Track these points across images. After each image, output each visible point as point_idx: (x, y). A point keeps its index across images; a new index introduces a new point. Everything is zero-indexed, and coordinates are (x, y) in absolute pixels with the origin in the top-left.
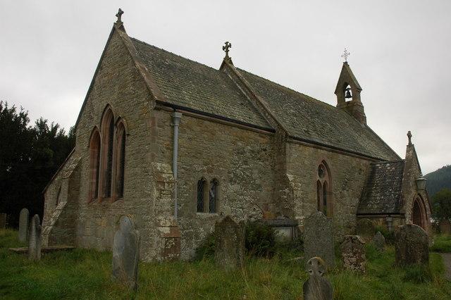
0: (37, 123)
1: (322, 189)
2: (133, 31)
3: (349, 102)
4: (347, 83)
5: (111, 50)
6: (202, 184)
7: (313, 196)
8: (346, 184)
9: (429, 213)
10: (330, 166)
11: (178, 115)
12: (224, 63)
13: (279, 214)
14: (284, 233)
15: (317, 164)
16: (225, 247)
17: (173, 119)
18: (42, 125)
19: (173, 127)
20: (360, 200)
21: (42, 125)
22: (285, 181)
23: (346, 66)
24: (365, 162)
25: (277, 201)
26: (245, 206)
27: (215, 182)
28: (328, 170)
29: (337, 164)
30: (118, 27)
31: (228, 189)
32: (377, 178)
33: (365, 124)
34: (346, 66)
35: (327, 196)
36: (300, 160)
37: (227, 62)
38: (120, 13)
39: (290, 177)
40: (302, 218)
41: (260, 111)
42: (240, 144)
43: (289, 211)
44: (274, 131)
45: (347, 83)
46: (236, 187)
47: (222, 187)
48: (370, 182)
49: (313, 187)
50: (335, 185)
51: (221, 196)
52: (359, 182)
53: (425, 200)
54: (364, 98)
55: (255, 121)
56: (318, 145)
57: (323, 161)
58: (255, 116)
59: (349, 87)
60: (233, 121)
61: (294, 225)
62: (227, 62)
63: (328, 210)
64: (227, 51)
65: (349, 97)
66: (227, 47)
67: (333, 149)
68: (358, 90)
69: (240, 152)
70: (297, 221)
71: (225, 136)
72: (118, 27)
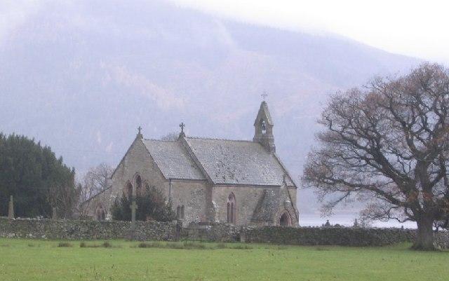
4: (262, 122)
23: (264, 103)
24: (259, 189)
25: (208, 214)
27: (183, 207)
30: (139, 136)
31: (188, 209)
32: (265, 202)
45: (262, 122)
47: (185, 208)
49: (225, 207)
56: (229, 185)
67: (238, 185)
72: (139, 136)
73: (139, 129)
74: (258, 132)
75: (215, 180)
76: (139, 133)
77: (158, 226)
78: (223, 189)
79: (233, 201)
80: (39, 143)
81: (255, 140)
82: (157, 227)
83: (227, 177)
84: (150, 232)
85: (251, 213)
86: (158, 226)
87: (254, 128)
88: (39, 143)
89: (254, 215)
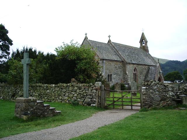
0: (35, 50)
1: (135, 75)
2: (90, 38)
3: (143, 46)
4: (143, 40)
5: (84, 44)
6: (109, 75)
7: (133, 77)
8: (141, 73)
9: (163, 79)
10: (137, 69)
11: (104, 61)
12: (109, 41)
13: (124, 81)
14: (127, 86)
15: (134, 69)
16: (117, 88)
17: (103, 62)
18: (39, 52)
19: (103, 64)
20: (145, 77)
21: (39, 52)
22: (126, 74)
23: (143, 34)
24: (147, 67)
25: (124, 78)
26: (117, 80)
27: (111, 75)
28: (137, 70)
29: (139, 68)
30: (86, 38)
31: (114, 76)
32: (150, 72)
33: (149, 53)
34: (143, 34)
35: (136, 77)
36: (130, 69)
37: (110, 41)
38: (86, 34)
39: (127, 73)
40: (130, 82)
41: (119, 56)
42: (151, 91)
43: (127, 81)
44: (123, 61)
45: (143, 40)
46: (115, 75)
47: (112, 76)
48: (148, 72)
49: (133, 75)
50: (138, 74)
51: (112, 78)
52: (145, 72)
53: (162, 77)
54: (149, 45)
55: (119, 59)
56: (134, 64)
57: (135, 68)
58: (118, 58)
59: (144, 41)
60: (114, 60)
61: (128, 84)
62: (109, 41)
63: (136, 81)
64: (109, 38)
65: (144, 44)
66: (109, 37)
67: (138, 64)
68: (147, 42)
69: (116, 67)
70: (129, 83)
71: (113, 64)
72: (86, 38)
73: (86, 34)
74: (141, 45)
75: (127, 60)
76: (86, 36)
77: (80, 88)
78: (132, 65)
79: (136, 72)
80: (17, 50)
81: (141, 48)
82: (78, 91)
83: (132, 60)
84: (71, 96)
85: (144, 77)
86: (80, 88)
87: (140, 44)
88: (17, 50)
89: (145, 79)
